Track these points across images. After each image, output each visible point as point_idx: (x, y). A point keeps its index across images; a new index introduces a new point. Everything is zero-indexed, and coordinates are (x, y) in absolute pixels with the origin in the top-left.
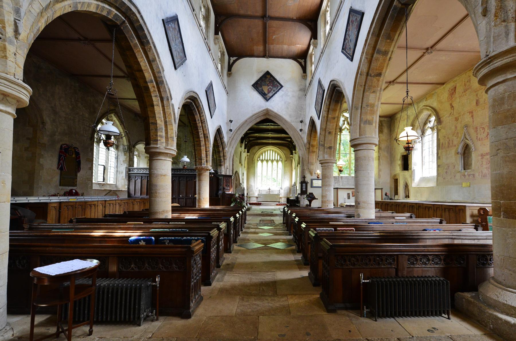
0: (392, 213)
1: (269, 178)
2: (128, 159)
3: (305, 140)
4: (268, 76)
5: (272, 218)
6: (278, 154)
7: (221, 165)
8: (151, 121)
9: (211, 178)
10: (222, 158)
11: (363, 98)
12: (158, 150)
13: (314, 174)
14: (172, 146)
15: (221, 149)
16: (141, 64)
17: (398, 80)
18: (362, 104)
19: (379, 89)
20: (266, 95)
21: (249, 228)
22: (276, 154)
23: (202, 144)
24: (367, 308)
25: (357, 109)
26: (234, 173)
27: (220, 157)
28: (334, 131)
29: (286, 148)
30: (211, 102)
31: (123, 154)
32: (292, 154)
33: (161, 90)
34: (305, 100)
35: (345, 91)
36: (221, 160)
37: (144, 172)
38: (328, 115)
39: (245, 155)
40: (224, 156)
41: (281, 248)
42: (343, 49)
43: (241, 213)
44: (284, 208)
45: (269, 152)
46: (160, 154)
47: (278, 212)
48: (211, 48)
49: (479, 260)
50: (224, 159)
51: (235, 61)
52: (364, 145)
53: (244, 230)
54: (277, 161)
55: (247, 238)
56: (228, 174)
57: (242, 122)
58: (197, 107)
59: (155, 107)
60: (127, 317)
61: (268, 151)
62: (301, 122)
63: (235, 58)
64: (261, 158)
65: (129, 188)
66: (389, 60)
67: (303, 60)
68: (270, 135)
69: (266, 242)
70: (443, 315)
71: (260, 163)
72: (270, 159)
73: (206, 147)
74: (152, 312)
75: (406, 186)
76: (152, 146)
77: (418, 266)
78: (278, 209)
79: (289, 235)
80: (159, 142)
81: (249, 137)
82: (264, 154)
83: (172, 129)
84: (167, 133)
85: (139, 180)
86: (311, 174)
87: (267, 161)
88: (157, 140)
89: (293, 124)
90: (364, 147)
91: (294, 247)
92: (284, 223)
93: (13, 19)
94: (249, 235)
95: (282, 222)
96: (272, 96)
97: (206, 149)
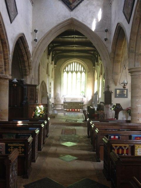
1: (75, 86)
5: (76, 128)
6: (82, 66)
7: (26, 75)
10: (27, 68)
15: (26, 58)
20: (71, 4)
22: (80, 66)
26: (41, 82)
27: (25, 67)
29: (89, 61)
30: (12, 9)
32: (94, 66)
36: (26, 70)
39: (51, 67)
40: (29, 66)
45: (74, 64)
47: (80, 121)
50: (29, 69)
53: (44, 149)
54: (81, 72)
61: (72, 63)
62: (106, 31)
64: (67, 70)
68: (75, 48)
71: (65, 73)
72: (74, 71)
73: (4, 54)
81: (56, 50)
82: (69, 66)
87: (72, 72)
92: (89, 137)
96: (77, 6)
97: (4, 57)
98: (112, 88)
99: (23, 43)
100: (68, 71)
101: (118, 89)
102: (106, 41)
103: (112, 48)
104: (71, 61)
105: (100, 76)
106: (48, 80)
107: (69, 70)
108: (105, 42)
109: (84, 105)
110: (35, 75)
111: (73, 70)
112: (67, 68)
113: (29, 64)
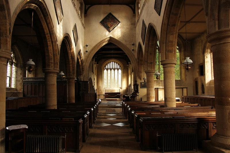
0: (189, 104)
2: (23, 72)
3: (136, 57)
4: (111, 16)
5: (115, 109)
7: (81, 75)
8: (46, 54)
9: (75, 84)
11: (166, 38)
12: (50, 71)
13: (142, 79)
14: (57, 68)
16: (43, 26)
17: (192, 21)
18: (166, 40)
19: (175, 32)
20: (109, 28)
21: (101, 115)
22: (117, 65)
23: (70, 63)
24: (159, 148)
25: (163, 43)
26: (89, 79)
27: (80, 69)
28: (153, 53)
31: (20, 69)
32: (128, 64)
33: (52, 38)
34: (135, 30)
35: (157, 31)
36: (80, 71)
37: (31, 80)
38: (149, 43)
41: (121, 126)
42: (155, 7)
43: (96, 106)
44: (123, 103)
46: (51, 72)
47: (119, 105)
48: (76, 5)
49: (214, 125)
51: (89, 8)
52: (168, 64)
54: (118, 69)
55: (100, 121)
56: (85, 80)
57: (94, 46)
58: (68, 42)
59: (49, 47)
60: (52, 151)
62: (133, 45)
63: (89, 6)
64: (106, 67)
65: (23, 91)
66: (179, 18)
67: (133, 5)
68: (112, 52)
69: (112, 123)
70: (194, 150)
71: (105, 71)
74: (63, 150)
75: (203, 86)
76: (47, 68)
77: (184, 129)
78: (118, 103)
79: (126, 119)
80: (50, 66)
82: (108, 64)
83: (57, 58)
84: (54, 61)
85: (30, 85)
86: (141, 79)
88: (49, 65)
89: (127, 46)
90: (169, 65)
91: (128, 125)
92: (122, 112)
93: (9, 28)
94: (101, 119)
95: (122, 111)
98: (139, 82)
99: (69, 44)
100: (107, 68)
101: (142, 83)
102: (133, 51)
103: (137, 56)
104: (111, 61)
105: (132, 73)
106: (93, 77)
107: (108, 68)
108: (133, 52)
109: (121, 95)
110: (86, 74)
111: (112, 68)
112: (106, 66)
113: (82, 67)
